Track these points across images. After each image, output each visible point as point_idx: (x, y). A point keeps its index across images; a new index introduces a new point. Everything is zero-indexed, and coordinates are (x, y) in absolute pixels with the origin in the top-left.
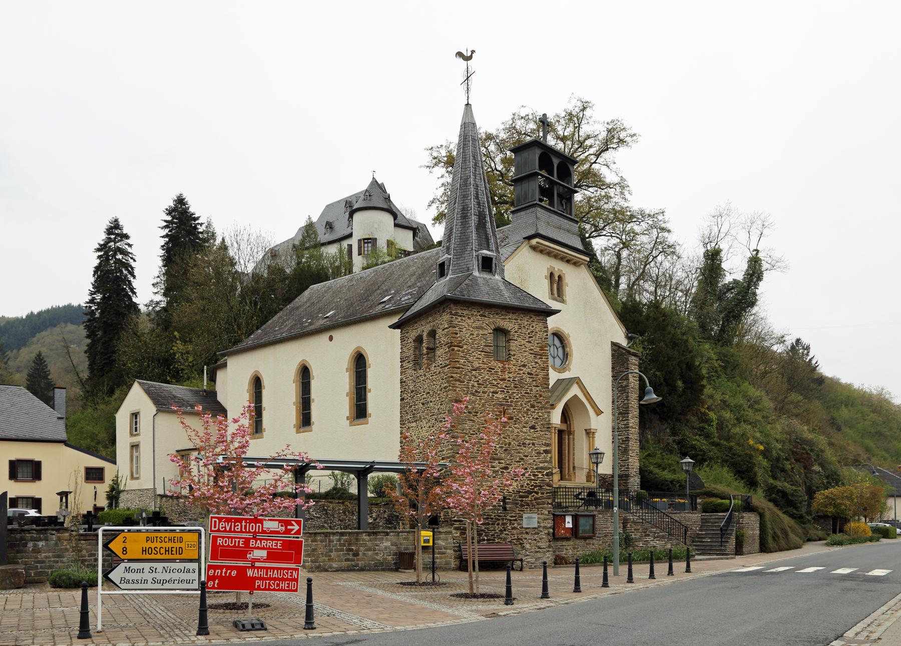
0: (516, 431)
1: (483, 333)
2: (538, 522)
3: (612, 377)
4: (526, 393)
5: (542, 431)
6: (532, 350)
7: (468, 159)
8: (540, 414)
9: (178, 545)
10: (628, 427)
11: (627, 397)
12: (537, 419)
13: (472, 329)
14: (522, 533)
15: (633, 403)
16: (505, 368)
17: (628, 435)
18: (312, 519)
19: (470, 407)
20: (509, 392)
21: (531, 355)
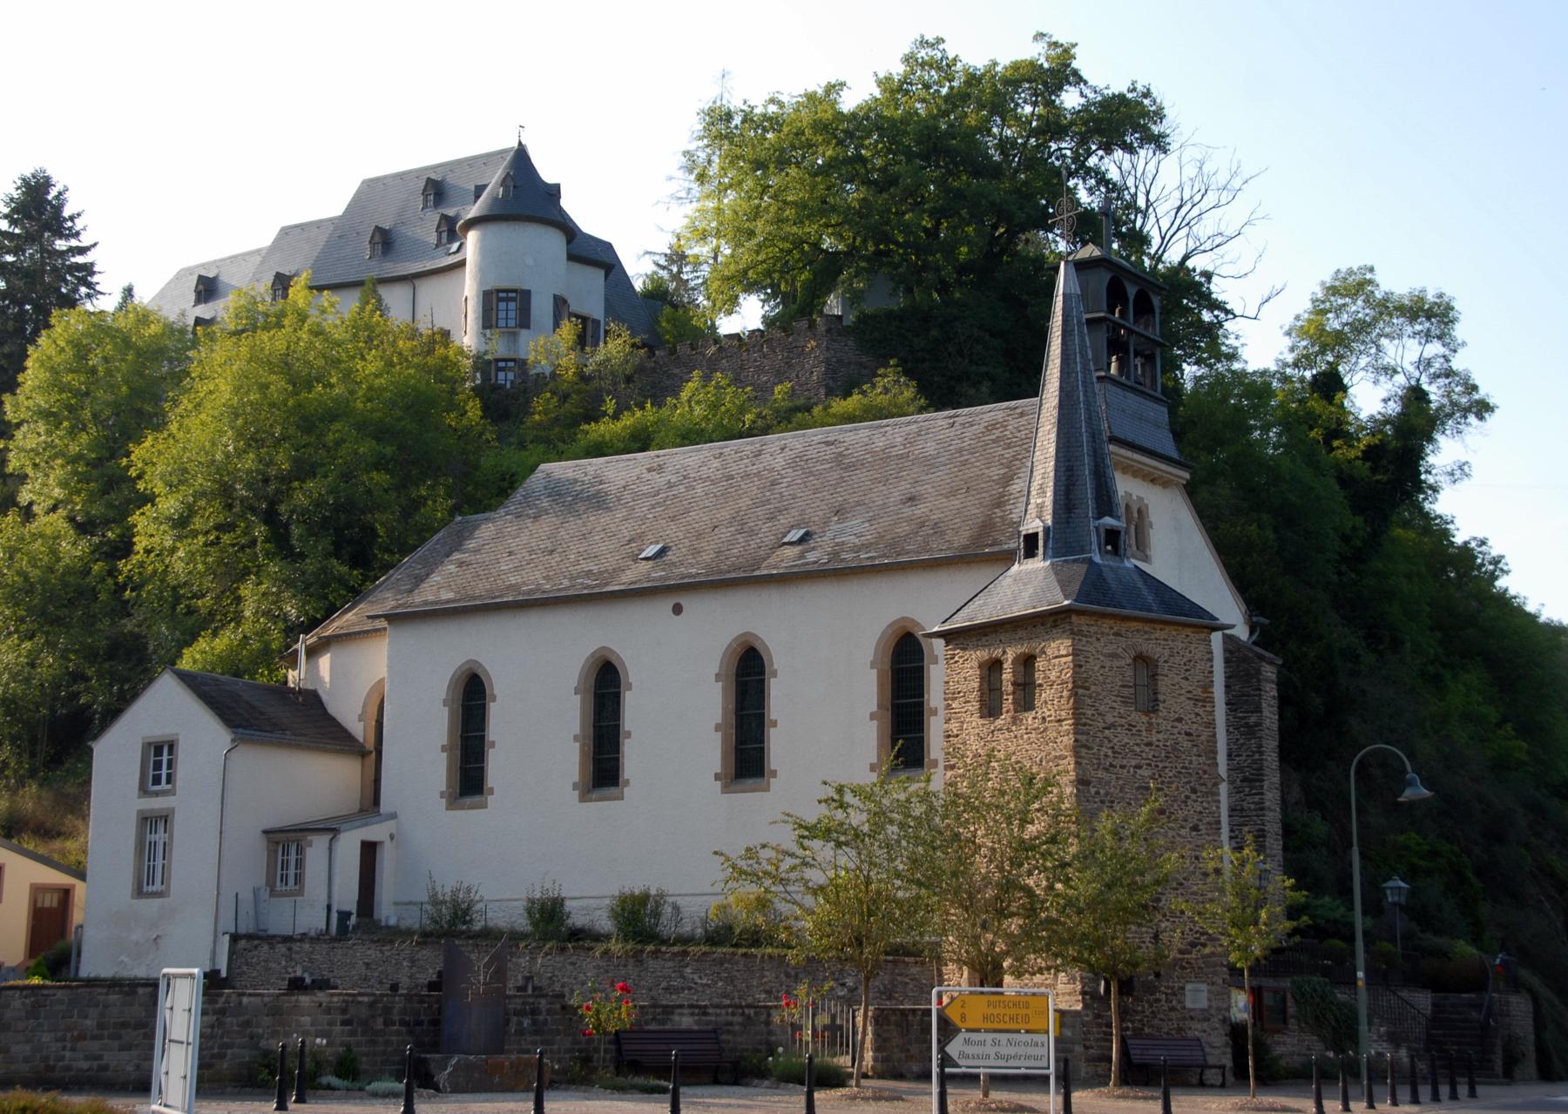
0: (1171, 833)
1: (1118, 664)
2: (1209, 1000)
3: (1227, 704)
4: (1183, 768)
5: (1209, 835)
6: (1189, 692)
7: (1072, 357)
8: (1205, 805)
9: (1023, 1012)
10: (1262, 809)
11: (1260, 746)
12: (1201, 813)
13: (1102, 658)
14: (1184, 1019)
15: (1269, 758)
16: (1151, 724)
17: (1263, 825)
18: (690, 989)
19: (1102, 791)
20: (1157, 766)
21: (1188, 702)
